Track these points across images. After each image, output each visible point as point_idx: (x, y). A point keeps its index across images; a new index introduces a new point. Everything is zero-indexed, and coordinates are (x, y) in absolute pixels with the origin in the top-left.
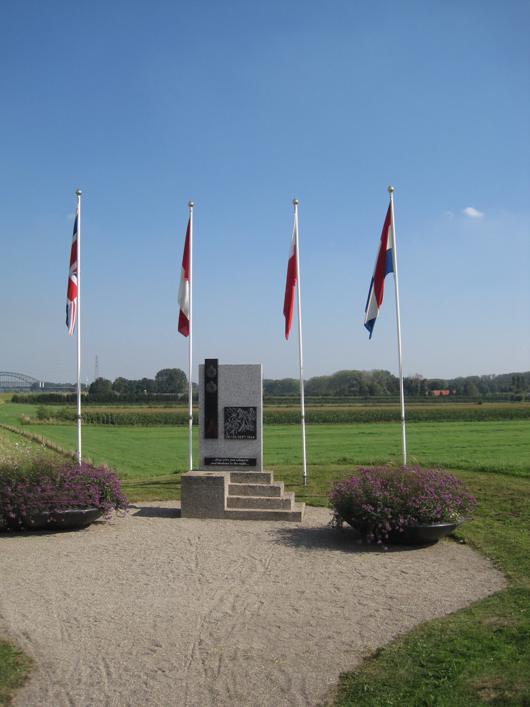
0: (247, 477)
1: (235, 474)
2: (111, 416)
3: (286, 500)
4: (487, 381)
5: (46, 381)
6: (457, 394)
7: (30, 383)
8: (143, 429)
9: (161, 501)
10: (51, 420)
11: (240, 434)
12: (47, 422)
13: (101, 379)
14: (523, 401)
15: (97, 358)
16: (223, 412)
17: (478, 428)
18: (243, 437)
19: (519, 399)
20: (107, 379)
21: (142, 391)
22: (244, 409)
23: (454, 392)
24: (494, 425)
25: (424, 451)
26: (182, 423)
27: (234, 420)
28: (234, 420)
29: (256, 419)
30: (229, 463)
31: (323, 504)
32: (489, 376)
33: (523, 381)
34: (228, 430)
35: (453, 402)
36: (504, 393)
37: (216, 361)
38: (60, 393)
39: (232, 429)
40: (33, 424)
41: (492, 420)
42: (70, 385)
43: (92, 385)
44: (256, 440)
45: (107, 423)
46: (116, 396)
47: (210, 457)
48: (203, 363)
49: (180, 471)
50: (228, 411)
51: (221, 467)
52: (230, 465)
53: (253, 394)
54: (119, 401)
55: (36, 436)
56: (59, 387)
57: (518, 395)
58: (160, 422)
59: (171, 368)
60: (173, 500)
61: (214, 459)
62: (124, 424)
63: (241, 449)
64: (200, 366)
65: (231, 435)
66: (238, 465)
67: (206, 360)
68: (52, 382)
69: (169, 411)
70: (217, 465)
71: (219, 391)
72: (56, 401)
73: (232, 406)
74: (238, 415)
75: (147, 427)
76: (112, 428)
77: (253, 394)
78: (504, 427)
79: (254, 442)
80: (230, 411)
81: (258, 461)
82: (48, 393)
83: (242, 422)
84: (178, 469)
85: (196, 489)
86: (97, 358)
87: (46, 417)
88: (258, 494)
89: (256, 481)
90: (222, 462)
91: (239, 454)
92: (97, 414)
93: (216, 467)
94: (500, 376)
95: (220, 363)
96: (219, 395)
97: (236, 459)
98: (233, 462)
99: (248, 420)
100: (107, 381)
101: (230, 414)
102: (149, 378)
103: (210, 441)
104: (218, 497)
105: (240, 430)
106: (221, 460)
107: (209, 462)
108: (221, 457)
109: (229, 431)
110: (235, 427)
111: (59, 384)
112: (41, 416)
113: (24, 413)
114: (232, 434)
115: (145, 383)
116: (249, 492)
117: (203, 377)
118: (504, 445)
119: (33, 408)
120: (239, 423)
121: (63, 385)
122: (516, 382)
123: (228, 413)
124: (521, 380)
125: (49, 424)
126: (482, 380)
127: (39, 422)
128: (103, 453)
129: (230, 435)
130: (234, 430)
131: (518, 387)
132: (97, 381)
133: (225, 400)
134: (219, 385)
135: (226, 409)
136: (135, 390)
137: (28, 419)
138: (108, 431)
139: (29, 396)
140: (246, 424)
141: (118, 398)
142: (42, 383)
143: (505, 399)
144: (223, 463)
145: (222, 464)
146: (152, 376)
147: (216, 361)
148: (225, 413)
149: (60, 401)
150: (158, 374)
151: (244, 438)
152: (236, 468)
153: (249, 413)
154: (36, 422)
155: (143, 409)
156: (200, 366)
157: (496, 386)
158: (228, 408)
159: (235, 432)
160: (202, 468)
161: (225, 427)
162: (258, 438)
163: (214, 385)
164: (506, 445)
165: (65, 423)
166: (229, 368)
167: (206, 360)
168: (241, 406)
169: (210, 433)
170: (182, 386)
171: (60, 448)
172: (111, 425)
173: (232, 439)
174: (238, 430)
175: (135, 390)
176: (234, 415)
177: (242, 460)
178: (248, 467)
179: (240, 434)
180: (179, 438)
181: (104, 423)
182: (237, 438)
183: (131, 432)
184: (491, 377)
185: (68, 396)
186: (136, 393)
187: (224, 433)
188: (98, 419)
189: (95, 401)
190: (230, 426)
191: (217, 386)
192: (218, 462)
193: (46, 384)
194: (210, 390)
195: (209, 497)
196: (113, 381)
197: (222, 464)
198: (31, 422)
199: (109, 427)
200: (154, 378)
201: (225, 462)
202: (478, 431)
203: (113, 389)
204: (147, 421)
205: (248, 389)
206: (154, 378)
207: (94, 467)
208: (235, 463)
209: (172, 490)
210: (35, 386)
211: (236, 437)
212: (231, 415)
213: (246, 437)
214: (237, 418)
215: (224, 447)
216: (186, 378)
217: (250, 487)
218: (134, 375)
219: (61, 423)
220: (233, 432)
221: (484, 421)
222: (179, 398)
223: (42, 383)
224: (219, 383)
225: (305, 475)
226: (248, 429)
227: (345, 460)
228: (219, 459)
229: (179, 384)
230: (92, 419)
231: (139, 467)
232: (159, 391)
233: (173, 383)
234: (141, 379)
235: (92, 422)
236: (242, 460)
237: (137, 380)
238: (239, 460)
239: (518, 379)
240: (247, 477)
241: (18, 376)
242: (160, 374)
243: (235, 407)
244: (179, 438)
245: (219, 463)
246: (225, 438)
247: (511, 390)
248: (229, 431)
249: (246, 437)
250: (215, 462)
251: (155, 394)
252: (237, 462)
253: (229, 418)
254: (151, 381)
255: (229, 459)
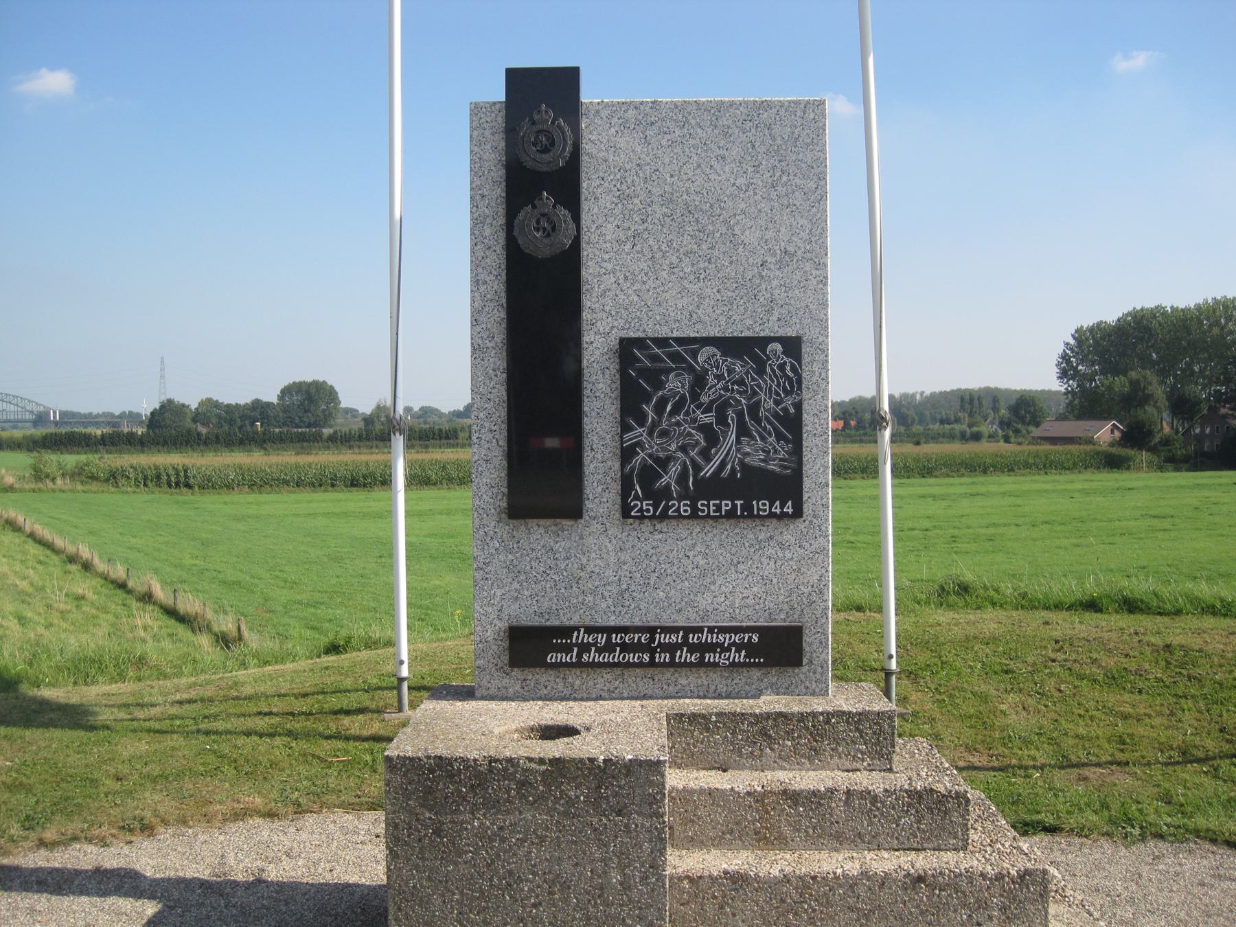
0: (764, 733)
1: (694, 718)
2: (186, 471)
3: (1024, 875)
4: (909, 403)
5: (64, 409)
6: (857, 428)
7: (31, 412)
8: (252, 497)
9: (271, 815)
10: (59, 481)
11: (714, 488)
12: (50, 485)
13: (170, 401)
14: (984, 440)
15: (162, 362)
16: (614, 367)
17: (936, 490)
18: (726, 505)
19: (977, 437)
20: (182, 401)
21: (253, 424)
22: (732, 346)
23: (853, 423)
24: (958, 485)
25: (848, 537)
26: (333, 485)
27: (676, 410)
28: (676, 410)
29: (798, 406)
30: (643, 652)
31: (1050, 820)
32: (913, 396)
33: (980, 403)
34: (645, 467)
35: (854, 442)
36: (947, 426)
37: (567, 79)
38: (90, 430)
39: (664, 463)
40: (22, 491)
41: (948, 476)
42: (112, 415)
43: (152, 414)
44: (800, 525)
45: (177, 484)
46: (199, 434)
47: (537, 622)
48: (497, 92)
49: (348, 640)
50: (640, 363)
51: (603, 680)
52: (652, 664)
53: (780, 265)
54: (205, 443)
55: (12, 514)
56: (90, 419)
57: (975, 429)
58: (286, 482)
59: (309, 379)
60: (331, 807)
61: (566, 631)
62: (213, 487)
63: (717, 574)
64: (476, 109)
65: (659, 496)
66: (701, 664)
67: (515, 78)
68: (75, 410)
69: (303, 459)
70: (579, 664)
71: (587, 251)
72: (80, 444)
73: (664, 332)
74: (699, 381)
75: (261, 493)
76: (185, 496)
77: (780, 265)
78: (982, 489)
79: (789, 533)
80: (655, 358)
81: (808, 639)
82: (63, 430)
83: (722, 420)
84: (344, 633)
85: (481, 835)
86: (162, 362)
87: (47, 476)
88: (839, 840)
89: (813, 757)
90: (609, 648)
91: (704, 602)
92: (157, 468)
93: (576, 678)
94: (933, 395)
95: (589, 94)
96: (589, 271)
97: (689, 630)
98: (672, 648)
99: (754, 409)
100: (183, 405)
101: (656, 378)
102: (265, 399)
103: (538, 534)
104: (626, 885)
105: (708, 470)
106: (602, 639)
107: (532, 649)
108: (601, 622)
109: (649, 475)
110: (683, 449)
111: (90, 414)
112: (39, 475)
113: (7, 469)
114: (666, 493)
115: (259, 409)
116: (787, 831)
117: (499, 173)
118: (1005, 525)
119: (23, 460)
120: (705, 429)
121: (98, 416)
122: (967, 406)
123: (642, 372)
124: (976, 402)
125: (54, 491)
126: (900, 402)
127: (33, 486)
128: (159, 550)
129: (648, 493)
130: (674, 469)
131: (971, 415)
132: (163, 407)
133: (620, 299)
134: (585, 219)
135: (627, 349)
136: (239, 423)
137: (10, 480)
138: (177, 502)
139: (24, 437)
140: (743, 431)
141: (203, 438)
142: (55, 413)
143: (951, 437)
144: (617, 656)
145: (607, 658)
146: (271, 396)
147: (567, 79)
148: (623, 372)
149: (88, 446)
150: (283, 391)
151: (731, 514)
152: (687, 679)
153: (761, 371)
154: (27, 487)
155: (255, 459)
156: (476, 109)
157: (927, 413)
158: (640, 343)
159: (682, 478)
160: (498, 682)
161: (627, 454)
162: (807, 509)
163: (563, 212)
164: (1010, 525)
165: (87, 487)
166: (645, 118)
167: (515, 78)
168: (714, 332)
169: (540, 479)
170: (330, 415)
171: (59, 543)
172: (184, 490)
173: (664, 516)
174: (697, 468)
175: (239, 423)
176: (676, 384)
177: (725, 639)
178: (756, 673)
179: (714, 488)
180: (326, 515)
181: (170, 486)
182: (694, 515)
183: (225, 503)
184: (918, 397)
185: (103, 435)
186: (240, 428)
187: (616, 487)
188: (158, 477)
189: (158, 444)
190: (654, 446)
191: (577, 218)
192: (585, 648)
193: (63, 414)
194: (538, 244)
195: (565, 886)
196: (194, 406)
197: (607, 658)
198: (17, 486)
199: (181, 494)
200: (275, 400)
201: (625, 648)
202: (934, 497)
203: (194, 420)
204: (258, 483)
205: (751, 237)
206: (275, 400)
207: (130, 584)
208: (683, 655)
209: (325, 748)
210: (41, 419)
211: (685, 509)
212: (659, 385)
213: (747, 507)
214: (695, 396)
215: (609, 564)
216: (337, 398)
217: (793, 797)
218: (237, 394)
219: (79, 487)
220: (669, 478)
221: (932, 476)
222: (325, 436)
223: (55, 413)
224: (585, 206)
225: (893, 665)
226: (755, 460)
227: (964, 589)
228: (590, 630)
229: (324, 411)
230: (145, 478)
231: (238, 583)
232: (285, 424)
233: (313, 408)
234: (249, 401)
235: (145, 485)
236: (725, 639)
237: (242, 402)
238: (706, 637)
239: (971, 401)
240: (764, 733)
241: (15, 402)
242: (286, 392)
243: (681, 341)
244: (326, 515)
245: (591, 656)
246: (626, 512)
247: (957, 420)
248: (649, 475)
249: (747, 507)
250: (567, 649)
251: (277, 430)
252: (692, 649)
253: (647, 398)
254: (269, 404)
255: (652, 630)
